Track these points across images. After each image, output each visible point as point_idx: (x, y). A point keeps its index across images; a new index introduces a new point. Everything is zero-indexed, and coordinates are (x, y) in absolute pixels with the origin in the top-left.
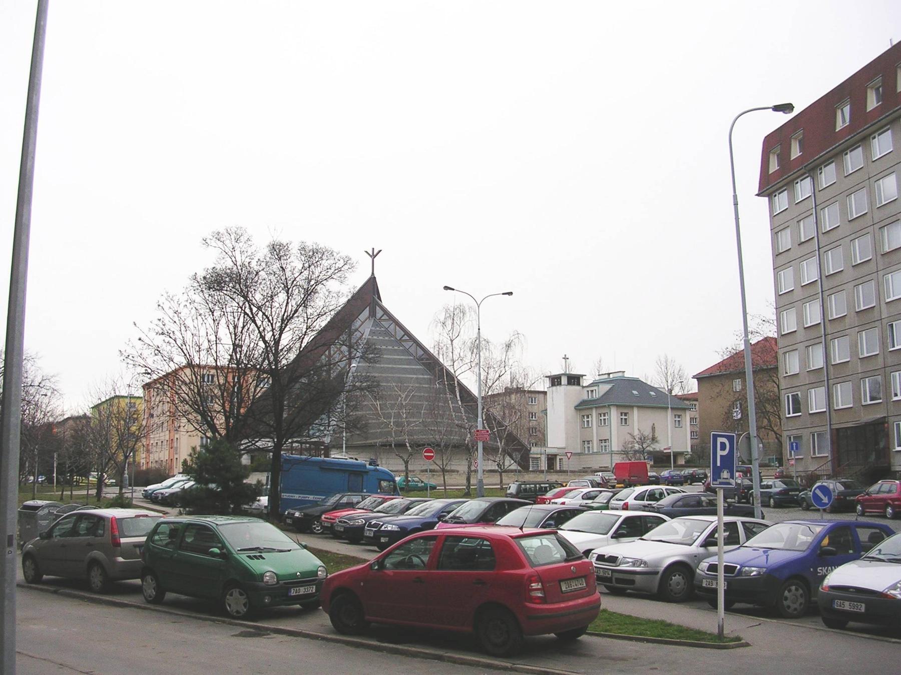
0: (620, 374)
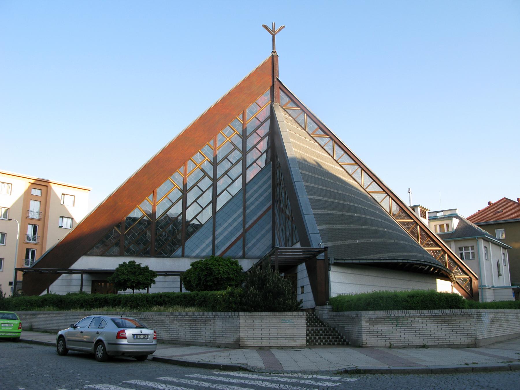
0: (453, 212)
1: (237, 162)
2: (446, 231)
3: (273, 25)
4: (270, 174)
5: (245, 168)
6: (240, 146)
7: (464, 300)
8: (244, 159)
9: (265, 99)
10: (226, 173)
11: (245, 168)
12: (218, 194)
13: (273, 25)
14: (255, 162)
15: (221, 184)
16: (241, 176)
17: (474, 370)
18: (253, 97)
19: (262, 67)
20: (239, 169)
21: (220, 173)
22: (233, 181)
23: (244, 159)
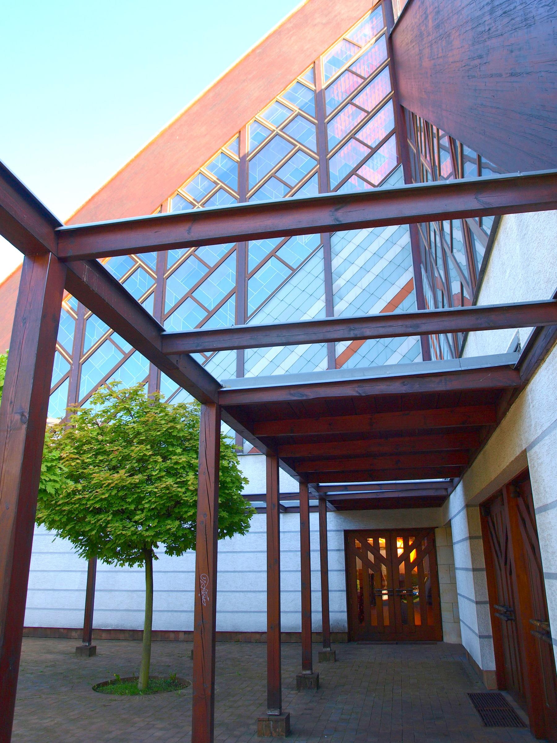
6: (312, 142)
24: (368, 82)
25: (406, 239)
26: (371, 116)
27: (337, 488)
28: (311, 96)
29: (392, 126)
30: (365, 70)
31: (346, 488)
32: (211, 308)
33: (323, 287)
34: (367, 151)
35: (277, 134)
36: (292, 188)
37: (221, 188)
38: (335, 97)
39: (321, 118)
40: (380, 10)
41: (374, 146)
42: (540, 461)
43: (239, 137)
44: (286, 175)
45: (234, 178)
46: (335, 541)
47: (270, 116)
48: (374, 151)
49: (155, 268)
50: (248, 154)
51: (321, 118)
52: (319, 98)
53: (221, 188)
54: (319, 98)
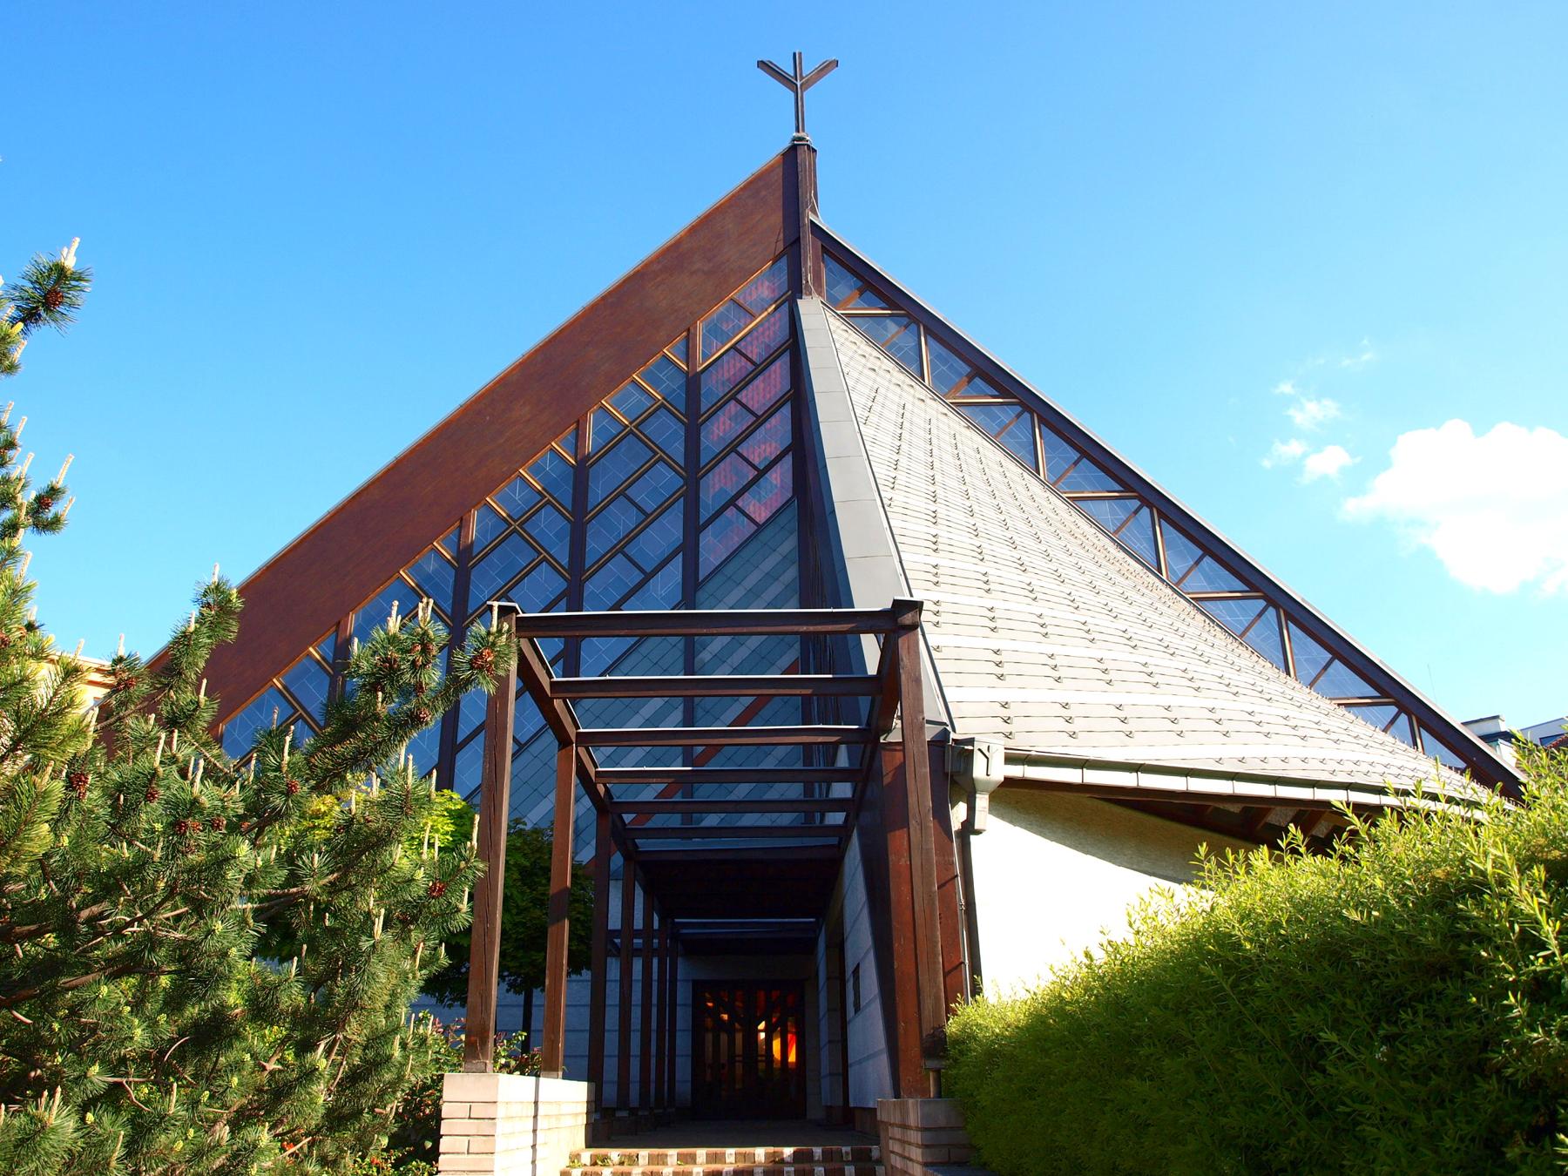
1: (663, 509)
2: (176, 734)
3: (796, 59)
4: (790, 544)
5: (694, 528)
6: (677, 450)
7: (1561, 1049)
8: (691, 495)
9: (761, 288)
10: (619, 549)
11: (694, 528)
12: (788, 459)
13: (796, 59)
14: (732, 502)
15: (717, 485)
16: (460, 738)
17: (918, 994)
18: (723, 279)
19: (754, 185)
20: (670, 530)
21: (596, 545)
22: (648, 577)
23: (691, 495)
24: (759, 369)
25: (681, 645)
26: (760, 420)
27: (692, 925)
28: (682, 380)
29: (788, 441)
30: (756, 352)
31: (705, 925)
32: (648, 570)
33: (681, 660)
34: (752, 473)
35: (631, 432)
36: (648, 516)
37: (549, 502)
38: (713, 388)
39: (693, 419)
40: (784, 262)
41: (648, 570)
42: (1100, 957)
43: (577, 429)
44: (640, 494)
45: (565, 494)
46: (683, 994)
47: (618, 407)
48: (761, 473)
49: (449, 611)
50: (589, 457)
51: (693, 419)
52: (693, 383)
53: (549, 502)
54: (693, 383)
